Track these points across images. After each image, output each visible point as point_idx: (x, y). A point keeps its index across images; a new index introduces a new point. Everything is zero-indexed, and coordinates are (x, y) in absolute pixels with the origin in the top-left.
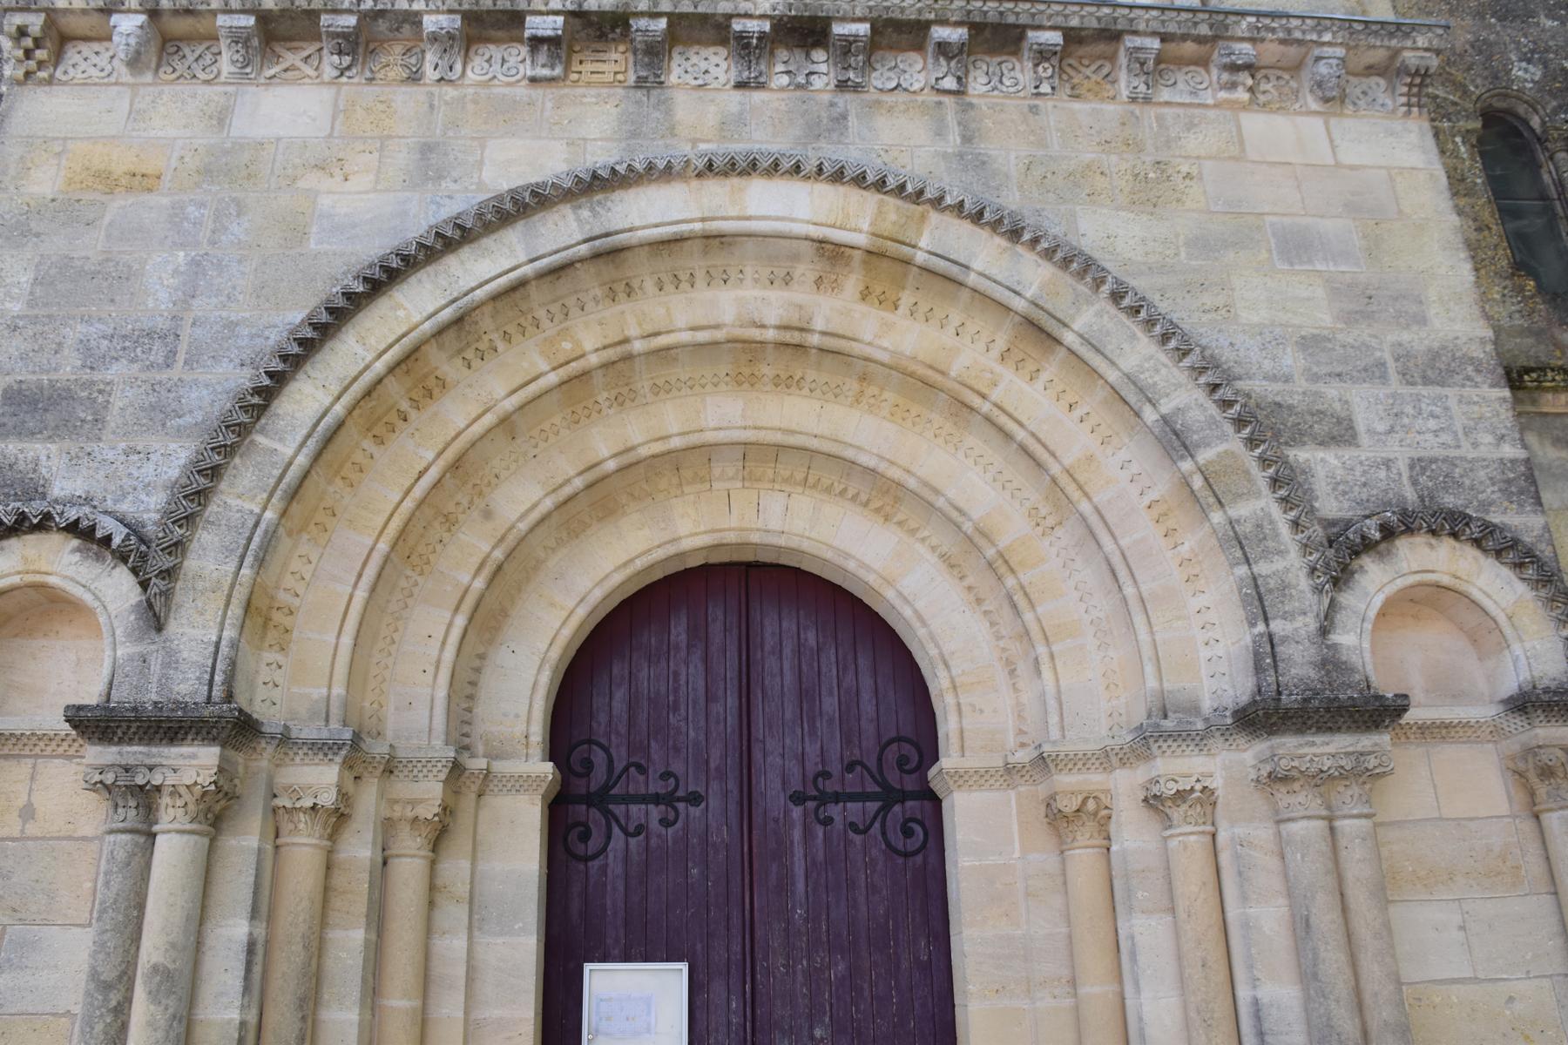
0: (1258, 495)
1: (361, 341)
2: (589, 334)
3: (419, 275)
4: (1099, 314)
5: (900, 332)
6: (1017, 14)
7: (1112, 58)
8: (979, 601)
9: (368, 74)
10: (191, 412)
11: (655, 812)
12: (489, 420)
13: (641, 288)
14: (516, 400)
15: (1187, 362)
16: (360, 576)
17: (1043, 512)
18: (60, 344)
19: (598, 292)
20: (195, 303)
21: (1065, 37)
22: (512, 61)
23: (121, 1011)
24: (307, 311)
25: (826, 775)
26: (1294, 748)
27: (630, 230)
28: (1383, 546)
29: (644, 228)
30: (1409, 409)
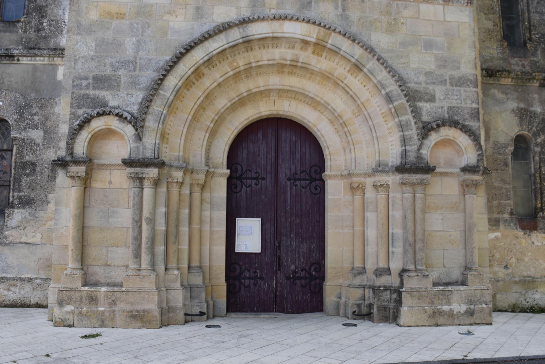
0: (408, 114)
1: (185, 65)
2: (241, 61)
4: (373, 64)
5: (322, 63)
8: (338, 132)
11: (254, 182)
12: (215, 84)
14: (222, 79)
15: (394, 79)
16: (185, 125)
17: (356, 112)
18: (105, 64)
19: (243, 50)
20: (140, 53)
23: (140, 227)
25: (296, 174)
26: (408, 177)
28: (437, 129)
30: (450, 93)
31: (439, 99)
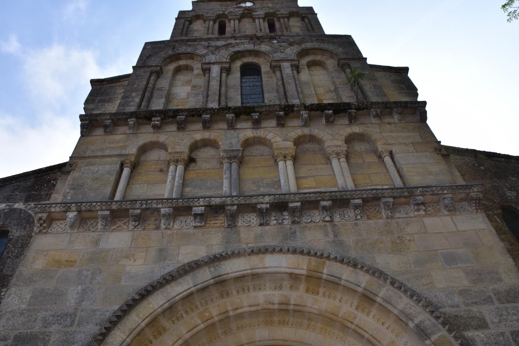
2: (215, 310)
3: (157, 292)
4: (388, 290)
5: (321, 302)
6: (347, 195)
7: (379, 205)
9: (143, 227)
10: (77, 342)
13: (232, 293)
14: (190, 334)
15: (421, 304)
18: (36, 319)
19: (217, 295)
20: (83, 303)
21: (363, 201)
22: (188, 221)
24: (120, 306)
27: (227, 274)
29: (232, 273)
30: (504, 313)
31: (492, 322)
